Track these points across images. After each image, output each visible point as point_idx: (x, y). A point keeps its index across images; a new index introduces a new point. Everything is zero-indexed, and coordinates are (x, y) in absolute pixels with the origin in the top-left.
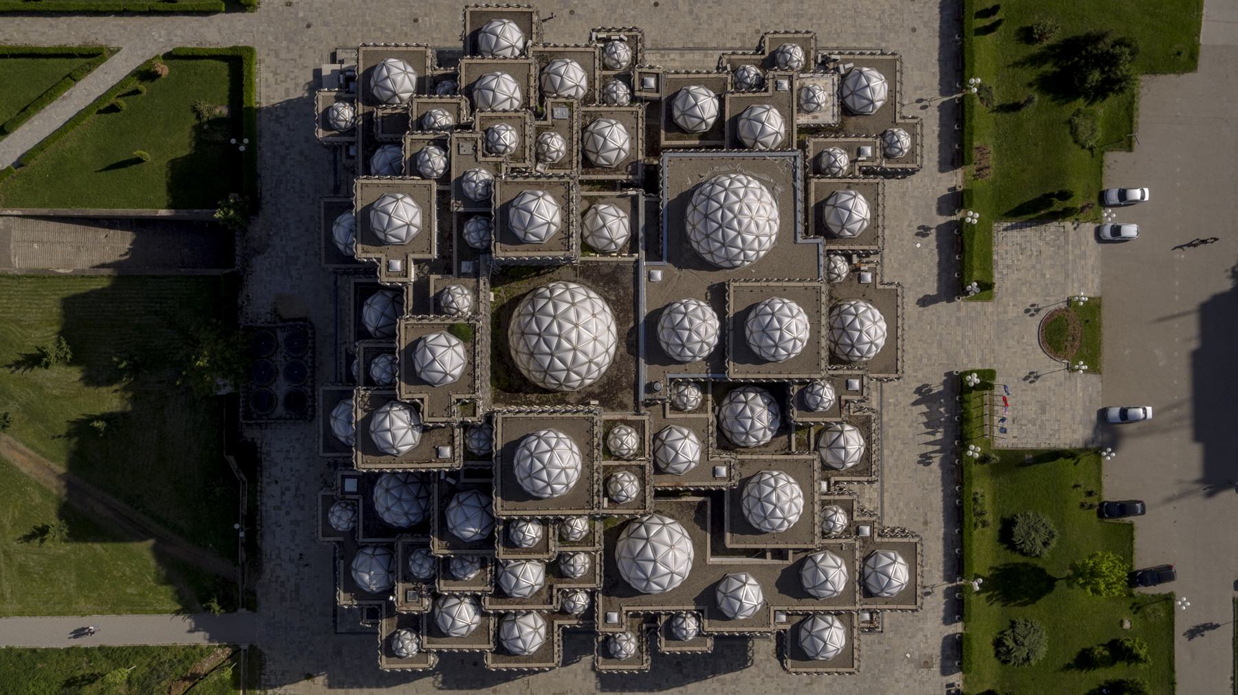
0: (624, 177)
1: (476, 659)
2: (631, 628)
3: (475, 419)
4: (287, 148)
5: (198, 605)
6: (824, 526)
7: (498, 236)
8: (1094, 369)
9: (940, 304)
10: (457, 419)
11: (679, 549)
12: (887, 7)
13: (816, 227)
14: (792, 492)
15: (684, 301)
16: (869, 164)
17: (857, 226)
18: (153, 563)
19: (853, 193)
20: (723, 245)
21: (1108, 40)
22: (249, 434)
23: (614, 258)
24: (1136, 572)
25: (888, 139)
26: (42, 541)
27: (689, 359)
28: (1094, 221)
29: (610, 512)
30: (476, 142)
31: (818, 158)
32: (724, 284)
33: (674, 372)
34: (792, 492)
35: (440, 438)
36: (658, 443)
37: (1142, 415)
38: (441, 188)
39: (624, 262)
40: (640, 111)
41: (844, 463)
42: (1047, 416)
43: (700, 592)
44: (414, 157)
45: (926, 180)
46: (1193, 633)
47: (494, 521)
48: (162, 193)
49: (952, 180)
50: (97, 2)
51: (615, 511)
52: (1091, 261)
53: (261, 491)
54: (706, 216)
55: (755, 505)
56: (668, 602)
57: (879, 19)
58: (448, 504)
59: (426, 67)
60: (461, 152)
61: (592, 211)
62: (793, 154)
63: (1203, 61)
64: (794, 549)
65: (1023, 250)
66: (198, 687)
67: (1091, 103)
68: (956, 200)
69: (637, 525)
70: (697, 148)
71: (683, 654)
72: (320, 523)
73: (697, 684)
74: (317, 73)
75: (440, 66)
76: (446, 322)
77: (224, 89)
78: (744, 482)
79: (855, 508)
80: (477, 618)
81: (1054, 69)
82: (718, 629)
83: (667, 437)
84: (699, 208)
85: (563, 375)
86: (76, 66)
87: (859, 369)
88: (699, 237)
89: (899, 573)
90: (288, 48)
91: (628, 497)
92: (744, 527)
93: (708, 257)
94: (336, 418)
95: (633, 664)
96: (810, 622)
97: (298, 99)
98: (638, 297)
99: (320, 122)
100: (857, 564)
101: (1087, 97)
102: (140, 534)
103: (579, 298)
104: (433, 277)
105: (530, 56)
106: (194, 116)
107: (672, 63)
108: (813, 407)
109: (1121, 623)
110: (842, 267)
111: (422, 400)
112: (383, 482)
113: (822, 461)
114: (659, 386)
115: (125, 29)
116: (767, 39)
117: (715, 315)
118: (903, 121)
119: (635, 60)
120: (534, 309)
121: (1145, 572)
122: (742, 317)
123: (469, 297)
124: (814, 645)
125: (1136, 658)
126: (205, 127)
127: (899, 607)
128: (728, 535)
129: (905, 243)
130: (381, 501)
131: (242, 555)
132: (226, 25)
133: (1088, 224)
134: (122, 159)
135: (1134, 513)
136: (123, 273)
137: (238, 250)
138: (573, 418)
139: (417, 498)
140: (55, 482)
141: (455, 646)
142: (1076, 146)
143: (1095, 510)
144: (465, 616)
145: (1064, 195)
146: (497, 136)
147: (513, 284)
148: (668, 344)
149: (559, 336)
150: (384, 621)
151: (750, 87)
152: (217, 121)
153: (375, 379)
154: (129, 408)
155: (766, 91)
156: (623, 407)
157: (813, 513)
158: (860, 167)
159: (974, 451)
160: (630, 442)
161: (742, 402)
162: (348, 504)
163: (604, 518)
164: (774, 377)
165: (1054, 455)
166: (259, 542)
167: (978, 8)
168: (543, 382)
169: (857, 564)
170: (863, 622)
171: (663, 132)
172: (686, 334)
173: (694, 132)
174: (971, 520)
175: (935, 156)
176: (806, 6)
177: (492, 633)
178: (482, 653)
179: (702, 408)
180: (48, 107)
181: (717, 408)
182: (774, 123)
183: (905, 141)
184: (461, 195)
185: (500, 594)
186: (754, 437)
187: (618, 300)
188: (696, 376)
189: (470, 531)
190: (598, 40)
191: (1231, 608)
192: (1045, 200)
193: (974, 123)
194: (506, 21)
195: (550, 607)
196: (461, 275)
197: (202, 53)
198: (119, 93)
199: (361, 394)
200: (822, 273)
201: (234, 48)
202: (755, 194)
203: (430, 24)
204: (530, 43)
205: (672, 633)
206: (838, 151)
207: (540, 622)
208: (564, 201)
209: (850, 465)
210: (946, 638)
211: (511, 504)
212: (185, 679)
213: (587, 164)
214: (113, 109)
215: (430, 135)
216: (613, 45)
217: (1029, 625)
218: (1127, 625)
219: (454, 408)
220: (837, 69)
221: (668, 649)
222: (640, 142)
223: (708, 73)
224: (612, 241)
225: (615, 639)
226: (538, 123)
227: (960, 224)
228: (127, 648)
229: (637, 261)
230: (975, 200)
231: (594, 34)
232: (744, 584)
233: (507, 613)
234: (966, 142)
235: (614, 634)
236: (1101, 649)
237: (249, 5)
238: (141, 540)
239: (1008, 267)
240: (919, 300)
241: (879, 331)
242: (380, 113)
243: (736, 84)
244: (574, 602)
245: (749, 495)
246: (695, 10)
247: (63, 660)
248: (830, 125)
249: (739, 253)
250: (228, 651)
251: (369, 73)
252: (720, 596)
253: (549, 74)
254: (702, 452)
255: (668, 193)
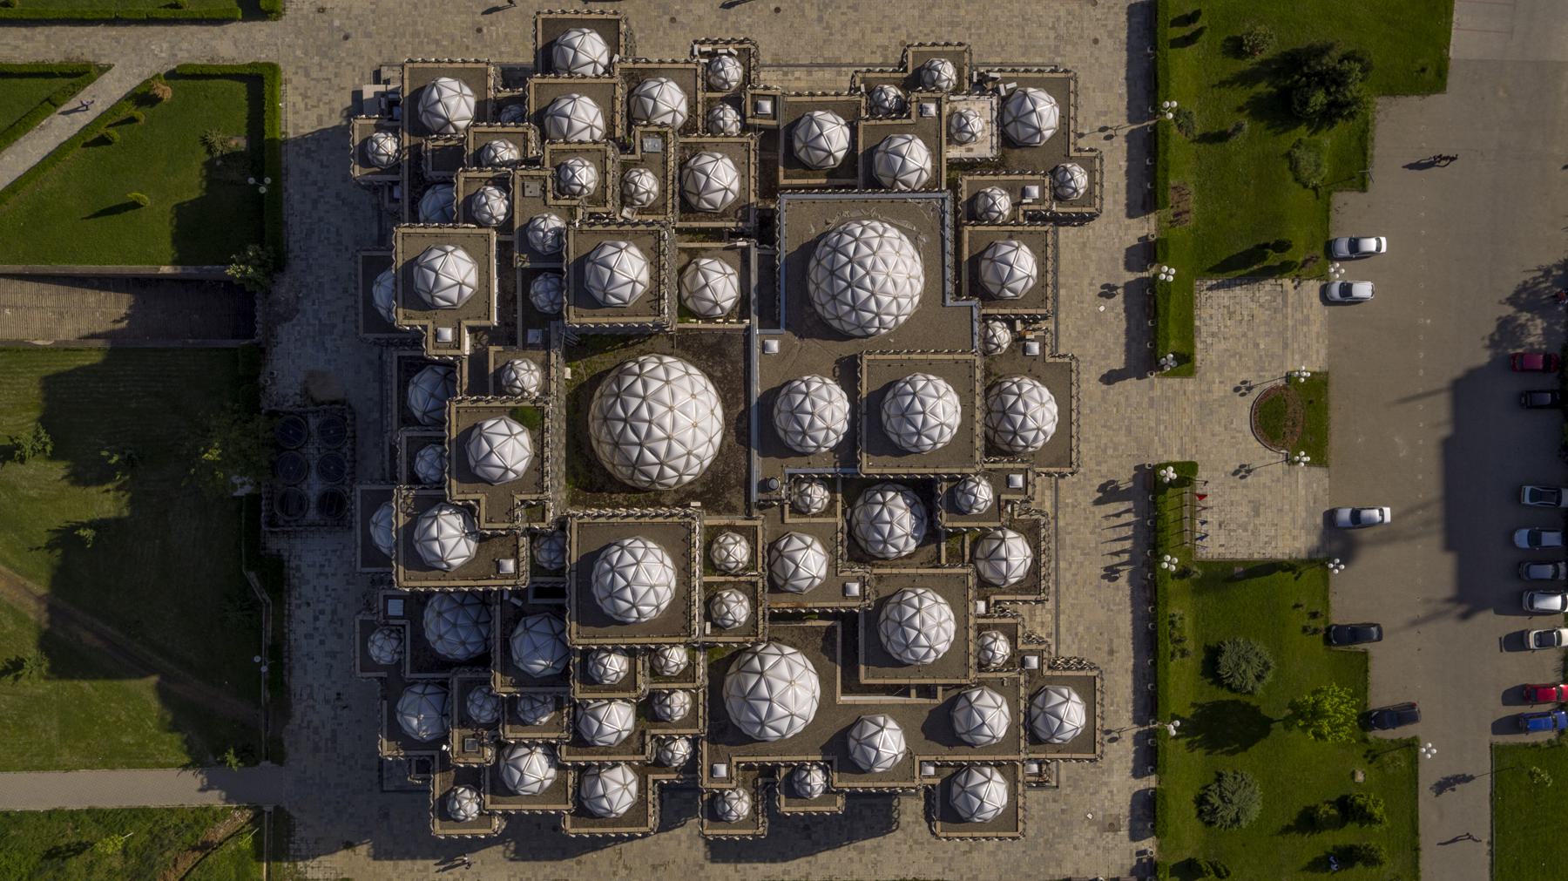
0: (734, 224)
1: (552, 823)
2: (744, 784)
3: (544, 525)
4: (321, 189)
5: (211, 757)
6: (981, 656)
7: (572, 297)
8: (1319, 460)
9: (1128, 381)
10: (521, 524)
11: (800, 685)
12: (1062, 13)
13: (971, 285)
14: (940, 614)
15: (806, 378)
16: (1036, 207)
17: (1020, 285)
18: (155, 705)
19: (1016, 243)
20: (853, 308)
21: (1333, 53)
22: (275, 544)
23: (720, 325)
24: (1371, 713)
25: (1059, 177)
26: (17, 678)
27: (812, 450)
28: (1319, 278)
29: (713, 639)
30: (545, 181)
31: (973, 199)
32: (855, 356)
33: (794, 466)
34: (940, 614)
35: (501, 549)
36: (774, 554)
37: (1378, 518)
38: (503, 238)
39: (732, 329)
40: (752, 143)
41: (1005, 578)
42: (1261, 520)
43: (828, 738)
44: (469, 200)
45: (1112, 227)
46: (1442, 786)
47: (568, 652)
48: (166, 246)
49: (1143, 228)
50: (145, 9)
51: (720, 639)
52: (1315, 328)
53: (289, 616)
54: (832, 273)
55: (895, 630)
56: (789, 752)
57: (1053, 28)
58: (512, 631)
59: (487, 88)
60: (527, 194)
61: (693, 266)
62: (940, 195)
63: (1453, 79)
64: (943, 685)
65: (1231, 315)
66: (210, 859)
67: (1315, 132)
68: (1146, 253)
69: (750, 656)
70: (822, 188)
71: (808, 815)
72: (358, 655)
73: (829, 852)
74: (357, 95)
75: (505, 87)
76: (508, 404)
77: (242, 115)
78: (882, 603)
79: (1020, 633)
80: (552, 772)
81: (1270, 89)
82: (851, 785)
83: (785, 547)
84: (824, 262)
85: (655, 471)
86: (56, 88)
87: (1023, 462)
88: (824, 299)
89: (1073, 714)
90: (320, 65)
91: (735, 621)
92: (883, 658)
93: (835, 324)
94: (376, 525)
95: (747, 828)
96: (964, 776)
97: (334, 128)
98: (749, 373)
99: (357, 158)
100: (1022, 703)
101: (1310, 123)
102: (143, 671)
103: (674, 374)
104: (493, 349)
105: (617, 73)
106: (203, 149)
107: (799, 81)
108: (966, 509)
109: (1353, 774)
110: (1002, 335)
111: (478, 501)
112: (434, 603)
113: (979, 575)
114: (775, 483)
115: (118, 42)
116: (910, 53)
117: (844, 395)
118: (1078, 154)
119: (747, 78)
120: (619, 388)
121: (1382, 712)
122: (878, 397)
123: (537, 374)
124: (969, 804)
125: (1370, 819)
126: (218, 163)
127: (1074, 756)
128: (862, 668)
129: (1085, 305)
130: (432, 626)
131: (266, 695)
132: (244, 36)
133: (1312, 282)
134: (114, 203)
135: (1369, 639)
136: (119, 345)
137: (259, 317)
138: (665, 524)
139: (476, 623)
140: (32, 604)
141: (525, 807)
142: (1297, 186)
143: (1321, 635)
144: (536, 770)
145: (1282, 246)
146: (570, 173)
147: (595, 358)
148: (786, 432)
149: (650, 422)
150: (437, 776)
151: (889, 112)
152: (232, 157)
153: (421, 476)
154: (126, 513)
155: (909, 117)
156: (731, 509)
157: (967, 640)
158: (1025, 212)
159: (1170, 563)
160: (738, 552)
161: (879, 503)
162: (392, 631)
163: (708, 647)
164: (917, 471)
165: (1269, 568)
166: (286, 679)
167: (1173, 14)
168: (631, 479)
169: (1022, 703)
170: (1030, 775)
171: (781, 168)
172: (807, 419)
173: (820, 168)
174: (1166, 649)
175: (1122, 198)
176: (962, 13)
177: (570, 791)
178: (559, 814)
179: (829, 510)
180: (22, 139)
181: (849, 511)
182: (917, 157)
183: (1080, 179)
184: (526, 246)
185: (581, 741)
186: (893, 545)
187: (725, 377)
188: (821, 470)
189: (540, 665)
190: (702, 54)
191: (1488, 757)
192: (1258, 252)
193: (1169, 157)
194: (586, 31)
195: (642, 758)
196: (527, 346)
197: (213, 71)
198: (110, 122)
199: (403, 494)
200: (976, 343)
201: (253, 65)
202: (892, 245)
203: (498, 34)
204: (616, 58)
205: (795, 790)
206: (996, 191)
207: (631, 776)
208: (653, 255)
209: (1013, 581)
210: (1136, 795)
211: (590, 630)
212: (194, 849)
213: (688, 208)
214: (103, 141)
215: (489, 173)
216: (719, 60)
217: (1239, 779)
218: (1360, 777)
219: (518, 512)
220: (996, 91)
221: (789, 809)
222: (752, 180)
223: (837, 94)
224: (716, 304)
225: (723, 797)
226: (624, 157)
227: (1153, 282)
228: (123, 810)
229: (748, 329)
230: (1171, 252)
231: (696, 47)
232: (882, 729)
233: (589, 766)
234: (1160, 180)
235: (722, 791)
236: (1327, 807)
237: (272, 12)
238: (142, 676)
239: (1213, 335)
240: (1103, 376)
241: (1047, 415)
242: (430, 146)
243: (871, 108)
244: (672, 752)
245: (887, 618)
246: (826, 17)
247: (43, 826)
248: (987, 159)
249: (873, 319)
250: (248, 814)
251: (417, 94)
252: (852, 743)
253: (639, 96)
254: (829, 565)
255: (787, 244)
